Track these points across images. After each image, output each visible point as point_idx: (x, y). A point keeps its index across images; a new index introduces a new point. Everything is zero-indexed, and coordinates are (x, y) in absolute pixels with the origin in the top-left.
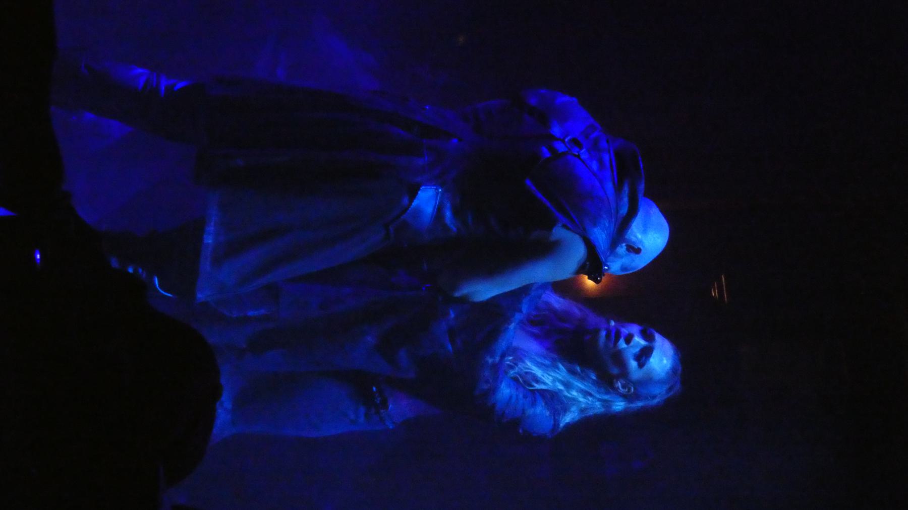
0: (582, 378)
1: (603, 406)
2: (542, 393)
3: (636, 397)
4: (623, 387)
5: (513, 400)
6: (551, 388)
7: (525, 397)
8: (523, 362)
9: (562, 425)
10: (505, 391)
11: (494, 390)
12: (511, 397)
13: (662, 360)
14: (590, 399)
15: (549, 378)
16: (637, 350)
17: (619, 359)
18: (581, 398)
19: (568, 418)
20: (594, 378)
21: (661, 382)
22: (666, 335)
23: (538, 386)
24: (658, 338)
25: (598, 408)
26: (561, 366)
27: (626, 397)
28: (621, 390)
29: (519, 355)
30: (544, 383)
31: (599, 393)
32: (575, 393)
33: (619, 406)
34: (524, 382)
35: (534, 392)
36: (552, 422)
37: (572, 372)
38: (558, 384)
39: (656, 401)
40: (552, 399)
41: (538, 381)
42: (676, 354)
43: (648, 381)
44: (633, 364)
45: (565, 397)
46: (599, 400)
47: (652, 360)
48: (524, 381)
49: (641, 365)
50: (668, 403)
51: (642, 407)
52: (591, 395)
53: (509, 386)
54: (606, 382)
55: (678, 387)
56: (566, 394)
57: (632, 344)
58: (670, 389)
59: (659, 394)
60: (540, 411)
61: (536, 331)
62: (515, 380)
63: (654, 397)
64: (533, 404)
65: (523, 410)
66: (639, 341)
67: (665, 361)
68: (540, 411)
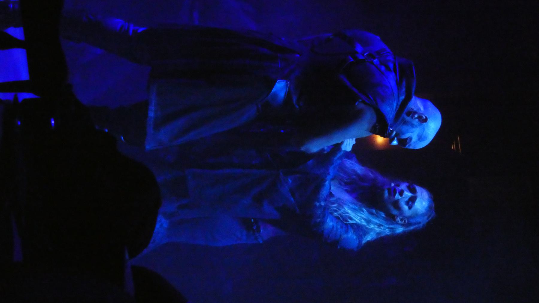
0: (377, 216)
1: (390, 231)
2: (352, 225)
3: (409, 224)
4: (401, 220)
5: (335, 229)
6: (360, 222)
7: (342, 227)
8: (343, 207)
9: (364, 242)
10: (330, 223)
11: (324, 222)
12: (333, 227)
13: (422, 203)
14: (382, 228)
15: (358, 216)
16: (407, 199)
17: (396, 205)
18: (375, 227)
19: (369, 238)
20: (384, 216)
21: (423, 215)
22: (422, 186)
23: (351, 222)
24: (418, 188)
25: (387, 232)
26: (364, 210)
27: (403, 225)
28: (400, 222)
29: (341, 203)
30: (354, 220)
31: (387, 224)
32: (372, 226)
33: (400, 230)
34: (343, 220)
35: (346, 225)
36: (358, 242)
37: (371, 214)
38: (363, 221)
39: (421, 225)
40: (358, 229)
41: (351, 219)
42: (430, 197)
43: (416, 215)
44: (406, 207)
45: (367, 228)
46: (388, 228)
47: (416, 204)
48: (343, 219)
49: (410, 208)
50: (429, 224)
51: (414, 230)
52: (382, 226)
53: (332, 221)
54: (391, 218)
55: (433, 214)
56: (367, 227)
57: (403, 196)
58: (429, 217)
59: (424, 221)
60: (351, 235)
61: (348, 189)
62: (337, 218)
63: (420, 223)
64: (347, 232)
65: (341, 236)
66: (408, 194)
67: (424, 203)
68: (351, 235)
